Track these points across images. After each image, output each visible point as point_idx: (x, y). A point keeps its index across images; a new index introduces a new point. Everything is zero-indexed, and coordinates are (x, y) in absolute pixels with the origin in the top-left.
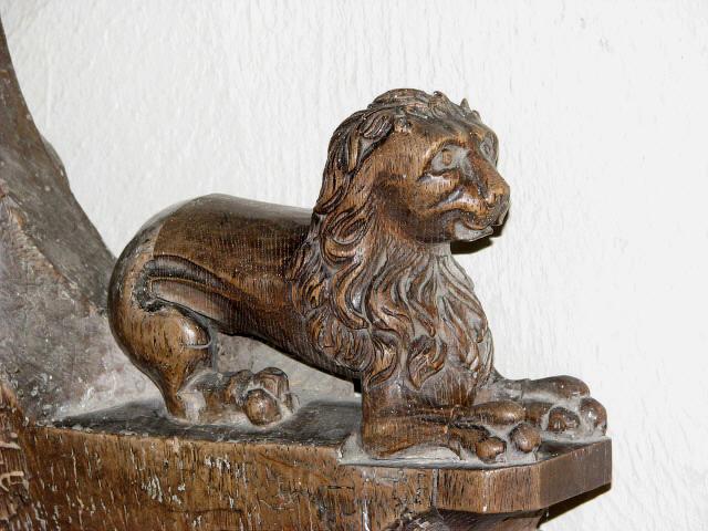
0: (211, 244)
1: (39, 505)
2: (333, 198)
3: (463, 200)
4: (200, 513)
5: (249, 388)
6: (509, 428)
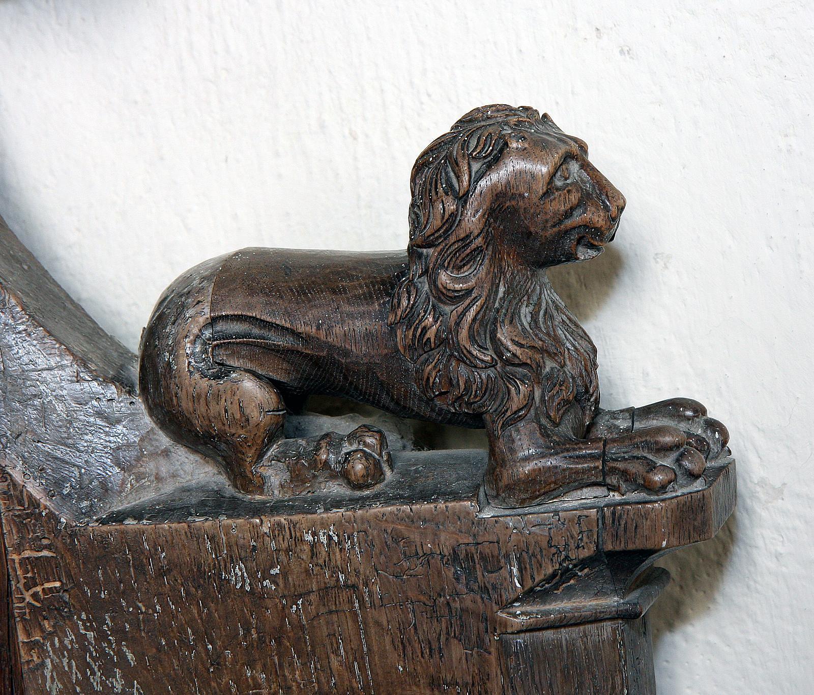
0: (282, 298)
1: (84, 616)
2: (441, 227)
3: (587, 216)
4: (300, 596)
5: (344, 451)
6: (674, 455)
